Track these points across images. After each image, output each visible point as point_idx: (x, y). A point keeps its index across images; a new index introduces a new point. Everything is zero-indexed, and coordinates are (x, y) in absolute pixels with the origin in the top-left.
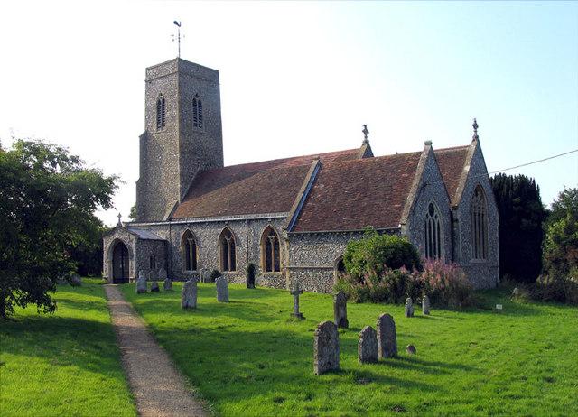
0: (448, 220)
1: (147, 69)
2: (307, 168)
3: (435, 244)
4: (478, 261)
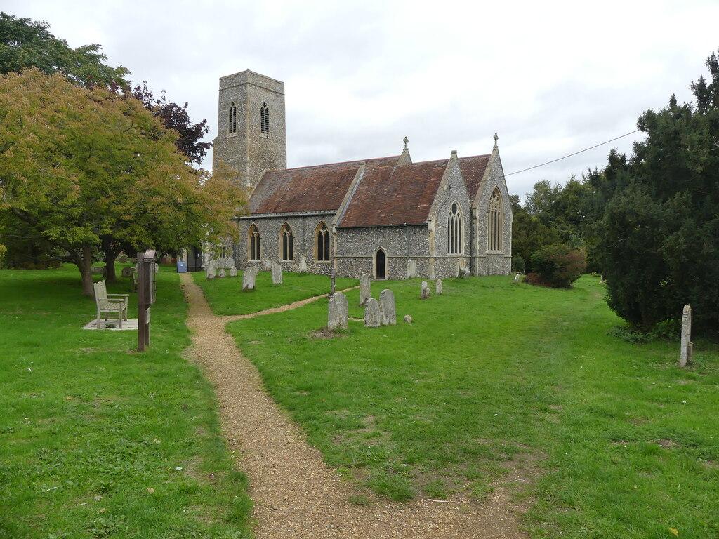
0: (468, 217)
1: (221, 79)
2: (353, 173)
3: (456, 238)
4: (493, 252)
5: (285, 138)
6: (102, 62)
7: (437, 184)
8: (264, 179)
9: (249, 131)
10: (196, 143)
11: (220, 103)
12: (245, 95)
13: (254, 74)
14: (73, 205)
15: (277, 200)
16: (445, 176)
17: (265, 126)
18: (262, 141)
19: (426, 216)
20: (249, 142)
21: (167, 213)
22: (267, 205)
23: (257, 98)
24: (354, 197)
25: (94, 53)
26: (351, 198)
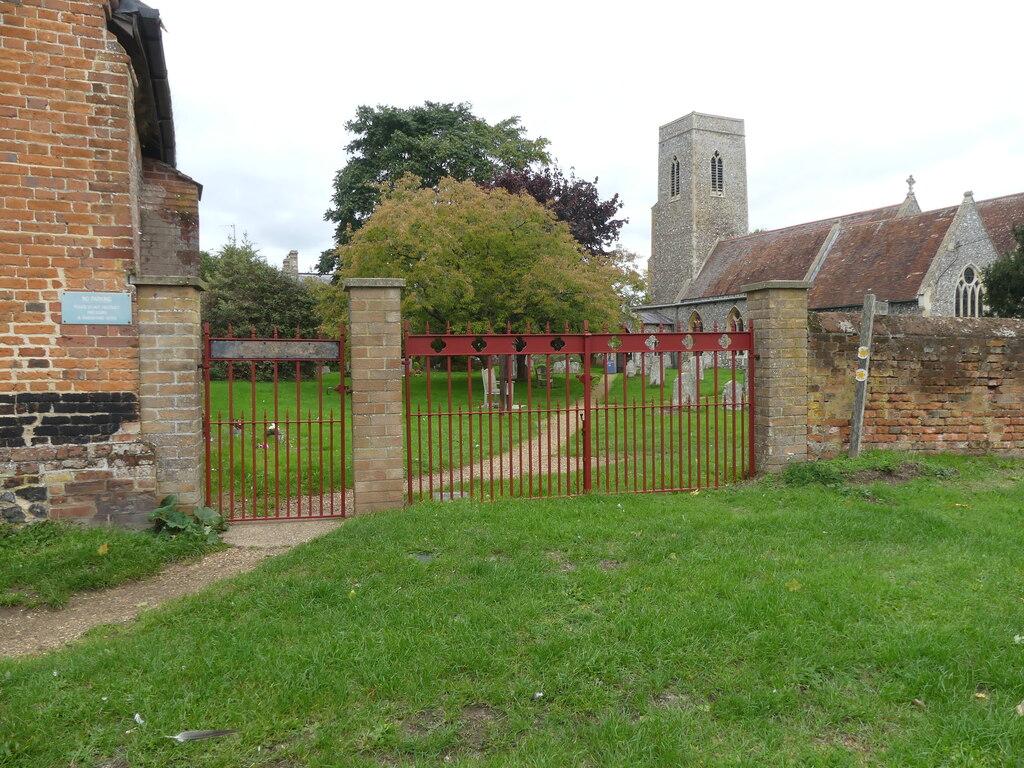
5: (745, 194)
6: (522, 136)
7: (938, 242)
8: (715, 252)
9: (695, 192)
10: (609, 221)
11: (660, 159)
12: (690, 144)
13: (702, 116)
14: (473, 302)
15: (730, 278)
16: (952, 228)
17: (717, 180)
18: (714, 202)
19: (916, 288)
20: (696, 206)
21: (552, 305)
22: (717, 285)
23: (705, 146)
24: (823, 267)
25: (514, 127)
26: (818, 269)
